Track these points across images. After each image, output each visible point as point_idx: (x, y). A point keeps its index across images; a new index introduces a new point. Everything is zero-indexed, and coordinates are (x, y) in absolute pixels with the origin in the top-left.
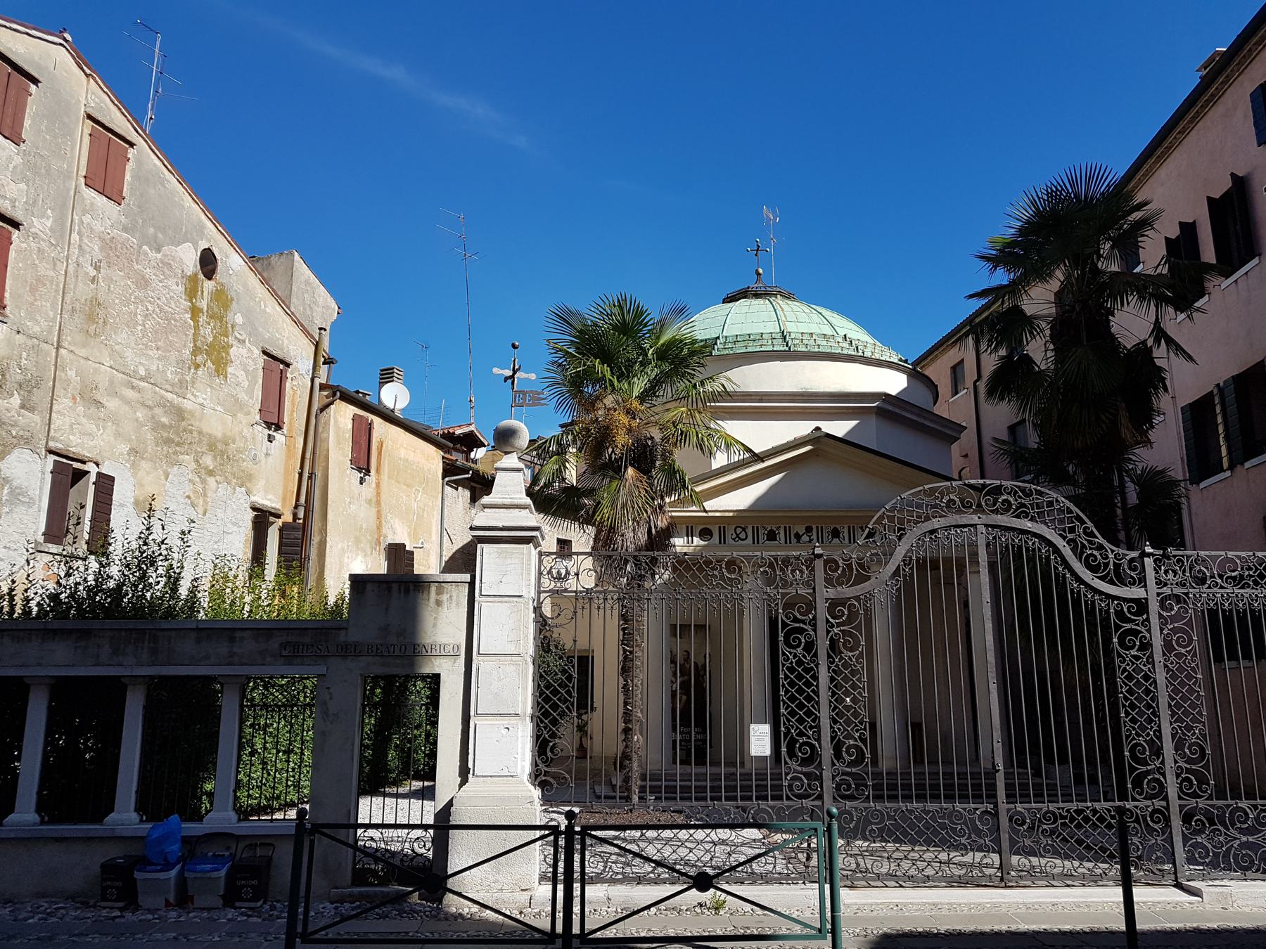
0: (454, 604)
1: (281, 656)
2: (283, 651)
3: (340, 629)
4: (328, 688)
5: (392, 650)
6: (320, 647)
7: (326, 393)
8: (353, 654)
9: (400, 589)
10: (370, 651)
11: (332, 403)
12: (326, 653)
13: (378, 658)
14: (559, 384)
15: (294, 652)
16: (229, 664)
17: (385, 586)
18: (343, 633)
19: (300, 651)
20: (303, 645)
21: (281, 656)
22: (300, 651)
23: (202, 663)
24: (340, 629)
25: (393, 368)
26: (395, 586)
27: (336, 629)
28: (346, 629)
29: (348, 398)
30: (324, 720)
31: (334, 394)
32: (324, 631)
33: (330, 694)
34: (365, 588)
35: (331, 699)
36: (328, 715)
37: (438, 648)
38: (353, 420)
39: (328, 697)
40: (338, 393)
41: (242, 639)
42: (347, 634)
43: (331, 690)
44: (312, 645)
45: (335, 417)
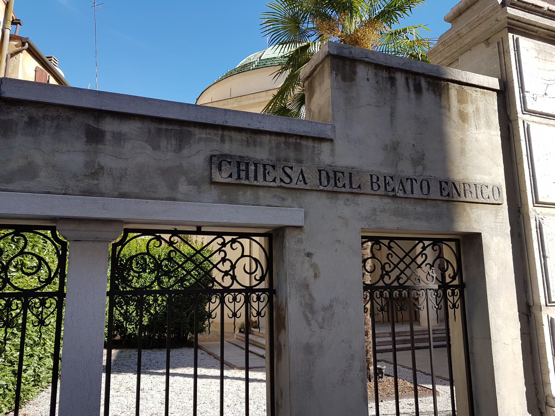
0: (483, 122)
1: (213, 183)
2: (215, 171)
3: (321, 140)
4: (309, 255)
5: (408, 187)
6: (288, 171)
7: (15, 43)
8: (347, 189)
9: (407, 83)
10: (375, 187)
11: (20, 51)
12: (301, 185)
13: (388, 200)
14: (277, 21)
15: (239, 178)
16: (87, 193)
17: (385, 74)
18: (325, 147)
19: (251, 175)
20: (256, 165)
21: (213, 183)
22: (251, 175)
23: (10, 186)
24: (321, 140)
25: (51, 57)
26: (400, 78)
27: (314, 139)
28: (331, 140)
29: (33, 52)
30: (308, 321)
31: (23, 44)
32: (292, 140)
33: (314, 266)
34: (355, 73)
35: (316, 276)
36: (313, 312)
37: (473, 189)
38: (36, 71)
39: (311, 273)
40: (27, 44)
41: (119, 138)
42: (333, 151)
43: (315, 259)
44: (273, 167)
45: (23, 64)
